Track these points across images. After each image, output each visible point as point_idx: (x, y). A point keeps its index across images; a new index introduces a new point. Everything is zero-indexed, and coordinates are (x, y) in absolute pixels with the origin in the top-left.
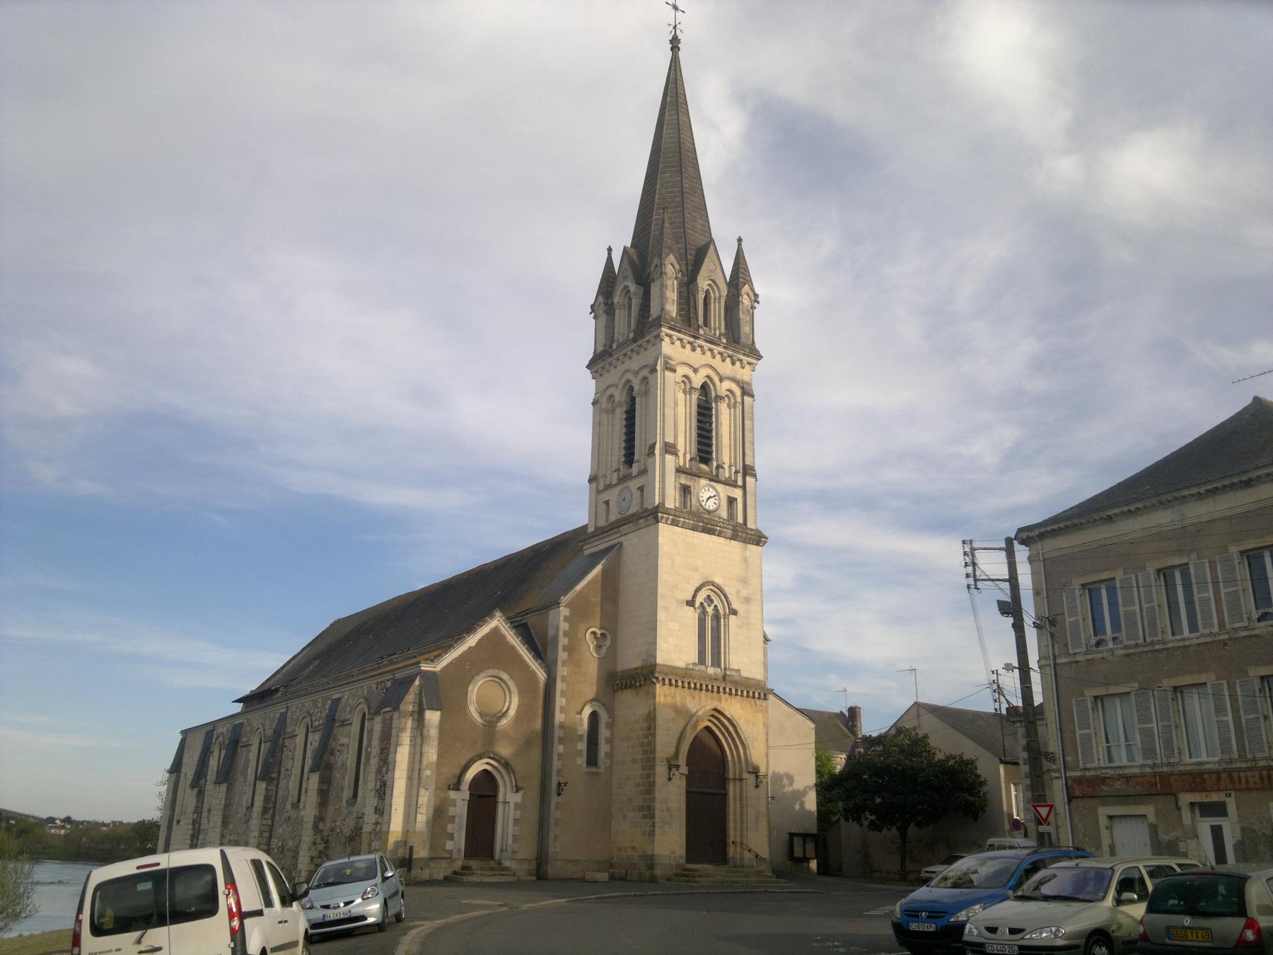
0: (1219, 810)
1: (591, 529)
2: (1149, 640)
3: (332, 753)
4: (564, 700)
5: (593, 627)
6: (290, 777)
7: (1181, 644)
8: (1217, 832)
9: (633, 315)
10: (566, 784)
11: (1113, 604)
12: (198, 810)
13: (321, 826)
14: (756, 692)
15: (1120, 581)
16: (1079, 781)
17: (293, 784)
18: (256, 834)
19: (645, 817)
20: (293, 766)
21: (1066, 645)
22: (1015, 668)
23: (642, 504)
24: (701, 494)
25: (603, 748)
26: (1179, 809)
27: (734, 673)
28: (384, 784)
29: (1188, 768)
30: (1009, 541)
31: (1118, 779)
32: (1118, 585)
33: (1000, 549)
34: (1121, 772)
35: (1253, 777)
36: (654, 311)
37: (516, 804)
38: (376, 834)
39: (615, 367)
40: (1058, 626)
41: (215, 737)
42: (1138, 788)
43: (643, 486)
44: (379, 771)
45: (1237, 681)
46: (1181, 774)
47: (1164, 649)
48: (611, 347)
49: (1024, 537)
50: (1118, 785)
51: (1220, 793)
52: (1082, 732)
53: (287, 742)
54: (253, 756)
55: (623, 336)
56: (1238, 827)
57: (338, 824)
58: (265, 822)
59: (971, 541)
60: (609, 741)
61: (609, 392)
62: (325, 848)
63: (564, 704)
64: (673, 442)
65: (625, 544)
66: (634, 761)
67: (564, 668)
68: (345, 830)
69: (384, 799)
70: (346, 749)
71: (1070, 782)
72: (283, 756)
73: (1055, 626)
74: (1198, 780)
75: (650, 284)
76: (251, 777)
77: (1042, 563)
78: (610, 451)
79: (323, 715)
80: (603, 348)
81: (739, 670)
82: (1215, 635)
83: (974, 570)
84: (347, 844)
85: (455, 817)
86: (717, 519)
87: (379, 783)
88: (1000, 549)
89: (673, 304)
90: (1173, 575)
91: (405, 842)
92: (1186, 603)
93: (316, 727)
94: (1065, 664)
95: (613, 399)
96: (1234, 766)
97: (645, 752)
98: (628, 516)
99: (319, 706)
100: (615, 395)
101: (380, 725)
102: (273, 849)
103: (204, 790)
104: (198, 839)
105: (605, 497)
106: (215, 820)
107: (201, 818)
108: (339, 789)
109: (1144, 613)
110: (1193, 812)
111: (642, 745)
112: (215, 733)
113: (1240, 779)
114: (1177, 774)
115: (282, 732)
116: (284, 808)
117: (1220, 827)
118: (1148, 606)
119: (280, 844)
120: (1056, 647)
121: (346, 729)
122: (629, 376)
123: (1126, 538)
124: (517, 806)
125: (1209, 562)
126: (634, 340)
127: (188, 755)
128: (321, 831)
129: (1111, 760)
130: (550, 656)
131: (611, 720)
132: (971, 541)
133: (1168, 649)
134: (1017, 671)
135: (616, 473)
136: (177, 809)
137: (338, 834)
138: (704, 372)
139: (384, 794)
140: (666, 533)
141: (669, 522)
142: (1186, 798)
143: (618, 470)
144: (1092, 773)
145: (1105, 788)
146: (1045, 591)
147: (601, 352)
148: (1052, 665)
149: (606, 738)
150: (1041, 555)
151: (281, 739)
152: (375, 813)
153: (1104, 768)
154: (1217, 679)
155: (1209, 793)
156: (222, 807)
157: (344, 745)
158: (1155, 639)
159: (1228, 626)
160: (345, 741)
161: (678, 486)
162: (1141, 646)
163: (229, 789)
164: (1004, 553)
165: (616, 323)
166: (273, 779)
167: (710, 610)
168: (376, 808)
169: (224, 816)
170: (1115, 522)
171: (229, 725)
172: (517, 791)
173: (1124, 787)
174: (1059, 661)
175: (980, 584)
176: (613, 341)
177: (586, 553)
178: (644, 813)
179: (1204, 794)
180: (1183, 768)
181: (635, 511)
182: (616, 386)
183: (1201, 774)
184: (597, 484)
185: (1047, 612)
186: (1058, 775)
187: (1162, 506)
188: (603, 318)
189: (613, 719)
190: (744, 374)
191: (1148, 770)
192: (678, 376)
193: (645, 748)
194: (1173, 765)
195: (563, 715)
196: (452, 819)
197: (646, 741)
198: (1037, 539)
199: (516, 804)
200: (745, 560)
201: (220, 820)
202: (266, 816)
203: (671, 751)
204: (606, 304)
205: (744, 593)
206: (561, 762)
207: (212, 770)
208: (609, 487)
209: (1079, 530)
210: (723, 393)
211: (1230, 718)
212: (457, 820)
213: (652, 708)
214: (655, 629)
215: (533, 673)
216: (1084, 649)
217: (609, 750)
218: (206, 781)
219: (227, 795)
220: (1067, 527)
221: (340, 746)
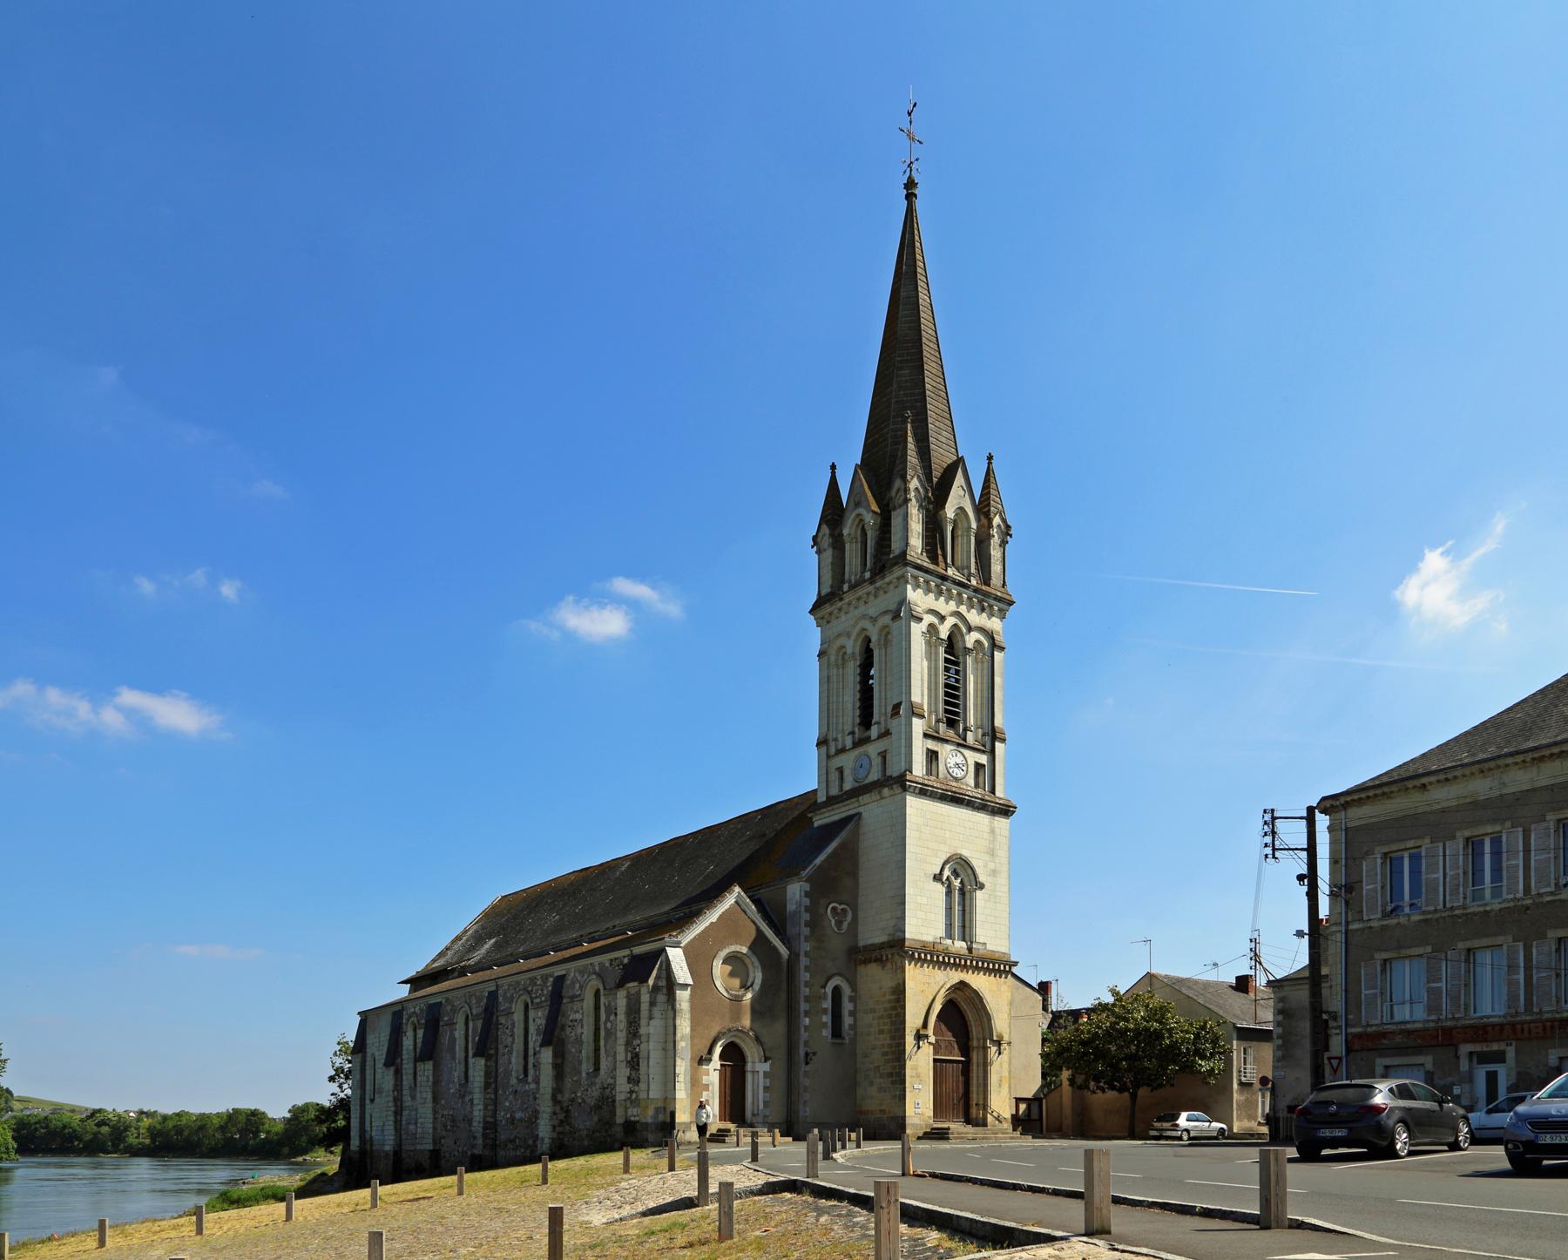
0: (1500, 1058)
1: (821, 798)
2: (1448, 905)
3: (563, 1028)
4: (808, 975)
5: (833, 902)
6: (511, 1053)
7: (1481, 909)
8: (1492, 1078)
9: (869, 551)
10: (814, 1054)
11: (1415, 873)
12: (398, 1086)
13: (559, 1097)
14: (1000, 967)
15: (1427, 849)
16: (1360, 1036)
17: (516, 1062)
18: (481, 1107)
19: (893, 1083)
20: (513, 1042)
21: (1361, 911)
22: (1306, 934)
23: (885, 771)
24: (949, 760)
25: (847, 1021)
26: (1458, 1057)
27: (980, 947)
28: (636, 1056)
29: (1472, 1022)
30: (1311, 810)
31: (1400, 1034)
32: (1423, 854)
33: (1301, 818)
34: (1403, 1027)
35: (1537, 1027)
36: (896, 547)
37: (765, 1073)
38: (631, 1102)
39: (846, 613)
40: (1354, 893)
41: (405, 1017)
42: (1419, 1041)
43: (885, 751)
44: (628, 1043)
45: (1534, 943)
46: (1464, 1027)
47: (1463, 914)
48: (841, 588)
49: (1328, 806)
50: (1398, 1039)
51: (1502, 1043)
52: (1367, 992)
53: (502, 1020)
54: (459, 1033)
55: (856, 575)
56: (1513, 1073)
57: (579, 1094)
58: (488, 1096)
59: (1273, 811)
60: (853, 1014)
61: (838, 643)
62: (566, 1117)
63: (808, 979)
64: (920, 702)
65: (865, 815)
66: (881, 1032)
67: (806, 944)
68: (588, 1100)
69: (639, 1070)
70: (580, 1025)
71: (1350, 1037)
72: (499, 1033)
73: (1351, 893)
74: (1481, 1032)
75: (890, 512)
76: (460, 1054)
77: (1344, 833)
78: (841, 711)
79: (545, 992)
80: (829, 590)
81: (985, 944)
82: (1519, 900)
83: (1273, 841)
84: (593, 1113)
85: (708, 1085)
86: (964, 787)
87: (629, 1054)
88: (1301, 818)
89: (918, 538)
90: (1482, 842)
91: (665, 1108)
92: (1491, 870)
93: (537, 1004)
94: (1357, 930)
95: (844, 650)
96: (1519, 1019)
97: (893, 1023)
98: (867, 784)
99: (538, 983)
100: (848, 646)
101: (625, 1000)
102: (501, 1121)
103: (402, 1068)
104: (401, 1115)
105: (837, 762)
106: (424, 1096)
107: (402, 1095)
108: (576, 1063)
109: (1448, 880)
110: (1471, 1060)
111: (890, 1016)
112: (405, 1013)
113: (1523, 1030)
114: (1460, 1028)
115: (495, 1010)
116: (508, 1082)
117: (1496, 1072)
118: (1452, 873)
119: (508, 1116)
120: (1350, 914)
121: (576, 1006)
122: (866, 624)
123: (1439, 807)
124: (766, 1075)
125: (1524, 831)
126: (872, 581)
127: (373, 1036)
128: (560, 1102)
129: (1392, 1017)
130: (658, 951)
131: (853, 994)
132: (1273, 811)
133: (1467, 914)
134: (1306, 937)
135: (850, 736)
136: (369, 1087)
137: (580, 1104)
138: (951, 621)
139: (638, 1065)
140: (915, 806)
141: (917, 791)
142: (1465, 1049)
143: (852, 733)
144: (1374, 1028)
145: (1385, 1042)
146: (1343, 861)
147: (827, 595)
148: (1343, 931)
149: (850, 1011)
150: (1343, 823)
151: (495, 1017)
152: (629, 1083)
153: (1387, 1024)
154: (1514, 941)
155: (1489, 1044)
156: (430, 1083)
157: (576, 1021)
158: (1455, 905)
159: (1534, 892)
160: (578, 1016)
161: (925, 749)
162: (1441, 911)
163: (436, 1067)
164: (1304, 822)
165: (847, 561)
166: (492, 1055)
167: (957, 883)
168: (629, 1078)
169: (434, 1093)
170: (1428, 790)
171: (422, 1005)
172: (766, 1061)
173: (1405, 1040)
174: (1351, 927)
175: (1278, 854)
176: (843, 582)
177: (816, 825)
178: (894, 1079)
179: (1484, 1044)
180: (1467, 1022)
181: (876, 779)
182: (848, 635)
183: (1484, 1027)
184: (827, 749)
185: (1343, 878)
186: (1338, 1031)
187: (1482, 775)
188: (828, 554)
189: (856, 992)
190: (995, 624)
191: (1432, 1025)
192: (923, 626)
193: (893, 1019)
194: (1458, 1019)
195: (808, 990)
196: (706, 1087)
197: (894, 1012)
198: (1341, 808)
199: (765, 1073)
200: (992, 831)
201: (430, 1096)
202: (489, 1091)
203: (920, 1022)
204: (832, 535)
205: (991, 866)
206: (807, 1034)
207: (407, 1050)
208: (842, 751)
209: (1389, 798)
210: (970, 644)
211: (1521, 977)
212: (710, 1088)
213: (901, 982)
214: (904, 903)
215: (775, 949)
216: (1379, 916)
217: (852, 1022)
218: (402, 1060)
219: (434, 1073)
220: (1376, 796)
221: (572, 1021)
